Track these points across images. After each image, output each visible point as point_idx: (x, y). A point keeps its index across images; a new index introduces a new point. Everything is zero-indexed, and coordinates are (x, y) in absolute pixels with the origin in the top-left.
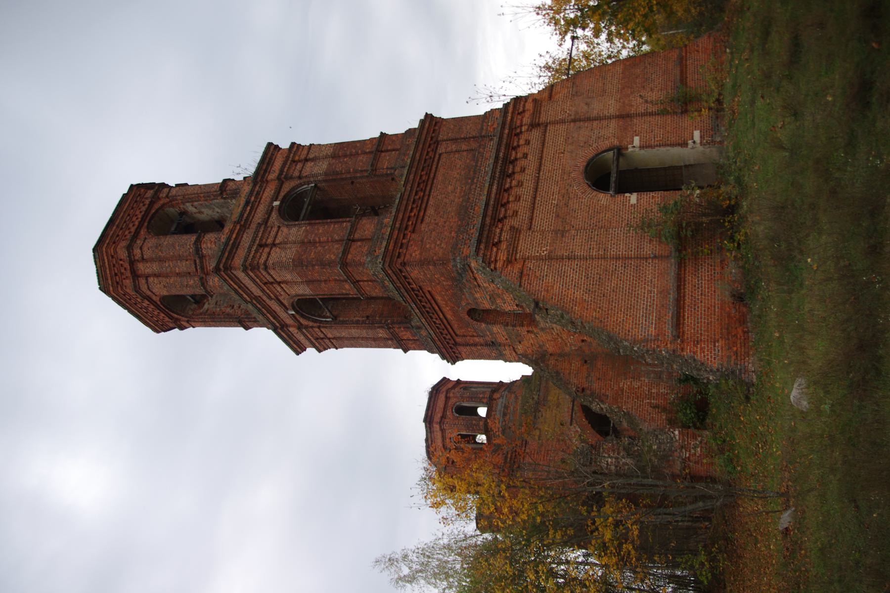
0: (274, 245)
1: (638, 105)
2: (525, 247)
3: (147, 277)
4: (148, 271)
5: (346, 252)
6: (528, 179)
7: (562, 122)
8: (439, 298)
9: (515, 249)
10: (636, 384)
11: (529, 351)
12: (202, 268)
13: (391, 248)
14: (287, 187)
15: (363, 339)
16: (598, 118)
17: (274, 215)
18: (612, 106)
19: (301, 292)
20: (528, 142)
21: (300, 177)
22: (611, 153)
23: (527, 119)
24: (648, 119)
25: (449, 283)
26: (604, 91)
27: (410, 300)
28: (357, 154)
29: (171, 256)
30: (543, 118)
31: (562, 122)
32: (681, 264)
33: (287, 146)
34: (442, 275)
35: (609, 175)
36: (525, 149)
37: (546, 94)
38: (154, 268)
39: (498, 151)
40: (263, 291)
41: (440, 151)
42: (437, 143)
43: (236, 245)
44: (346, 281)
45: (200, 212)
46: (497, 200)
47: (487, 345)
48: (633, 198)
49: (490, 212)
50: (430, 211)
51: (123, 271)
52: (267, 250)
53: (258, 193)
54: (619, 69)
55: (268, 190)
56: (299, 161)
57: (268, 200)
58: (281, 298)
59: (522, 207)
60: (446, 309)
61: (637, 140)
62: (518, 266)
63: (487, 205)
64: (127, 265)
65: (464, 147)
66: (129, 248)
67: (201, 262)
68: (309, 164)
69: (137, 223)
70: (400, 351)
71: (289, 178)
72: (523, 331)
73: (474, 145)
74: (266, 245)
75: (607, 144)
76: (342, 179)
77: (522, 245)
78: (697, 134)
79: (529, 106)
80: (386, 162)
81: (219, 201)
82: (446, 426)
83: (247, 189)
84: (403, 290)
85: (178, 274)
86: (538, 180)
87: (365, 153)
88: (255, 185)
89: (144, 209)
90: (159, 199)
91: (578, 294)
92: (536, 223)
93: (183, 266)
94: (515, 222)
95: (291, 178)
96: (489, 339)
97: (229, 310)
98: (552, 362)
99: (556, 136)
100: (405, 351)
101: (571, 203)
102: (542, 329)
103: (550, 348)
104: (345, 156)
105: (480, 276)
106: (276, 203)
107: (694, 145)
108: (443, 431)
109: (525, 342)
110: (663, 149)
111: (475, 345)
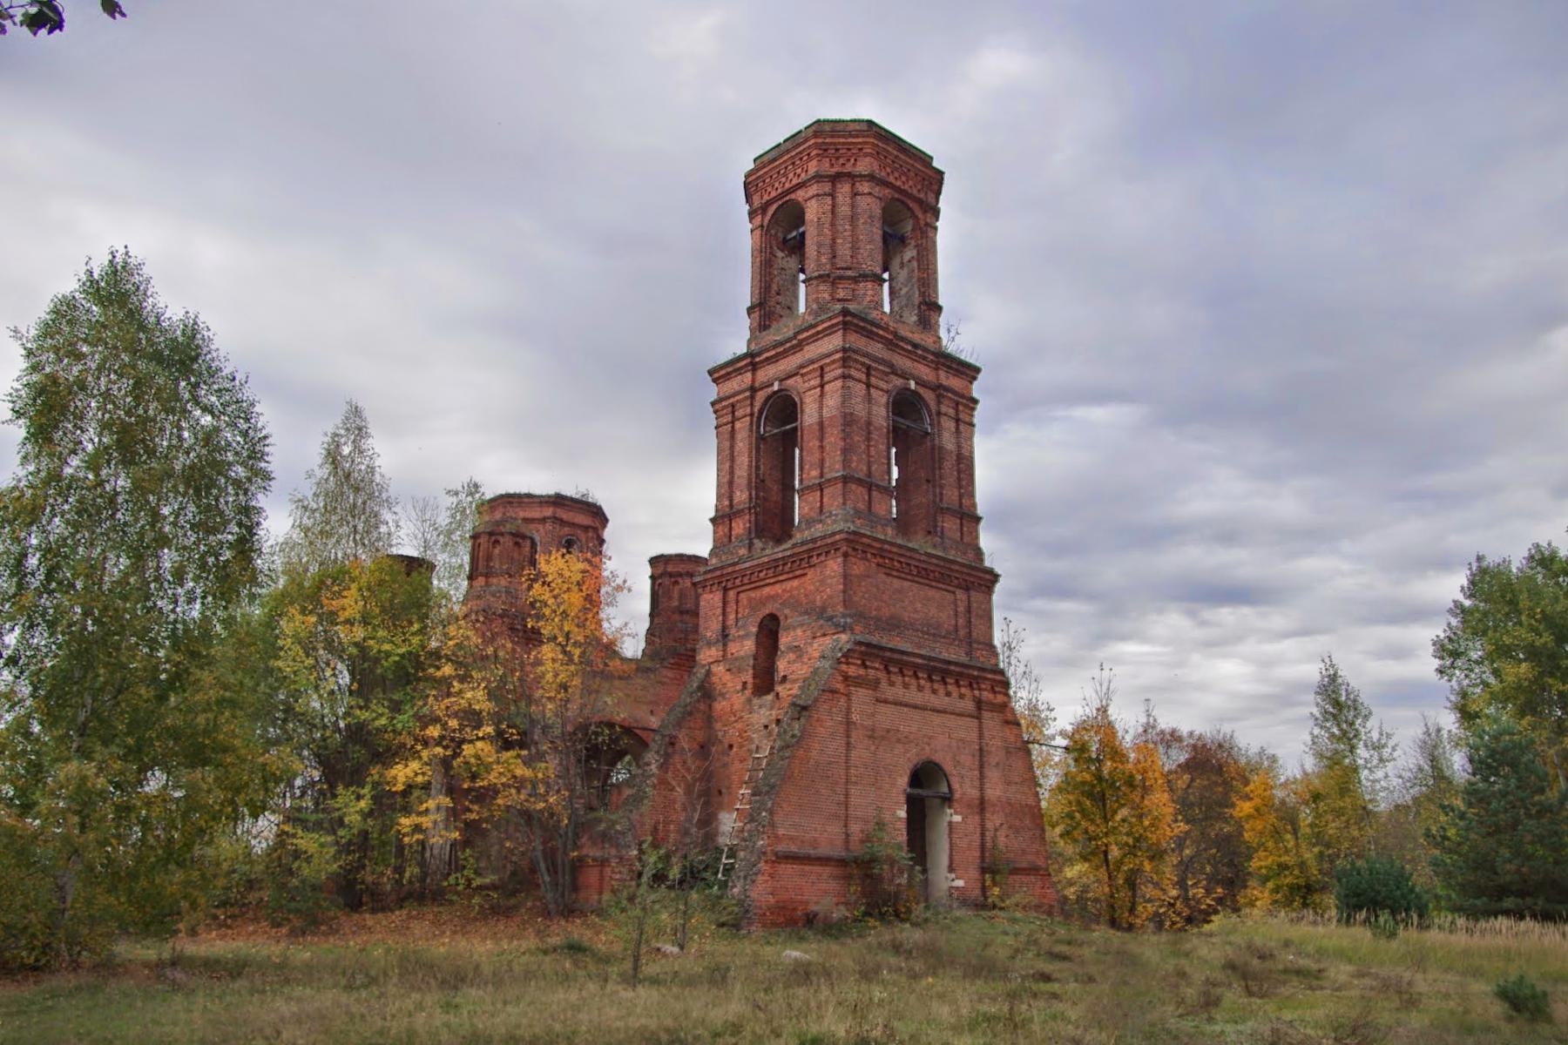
0: (868, 385)
1: (993, 821)
2: (861, 695)
3: (832, 195)
4: (840, 199)
5: (859, 482)
6: (925, 697)
7: (981, 736)
8: (796, 583)
9: (859, 685)
10: (678, 806)
11: (714, 679)
12: (841, 278)
13: (865, 540)
14: (929, 396)
15: (732, 472)
16: (982, 777)
17: (899, 382)
18: (994, 791)
19: (807, 410)
20: (962, 696)
21: (939, 413)
22: (946, 790)
23: (987, 695)
24: (978, 831)
25: (818, 604)
26: (1009, 783)
27: (796, 550)
28: (960, 487)
29: (844, 209)
30: (986, 715)
31: (981, 736)
32: (842, 862)
33: (975, 395)
34: (830, 597)
35: (926, 784)
36: (955, 694)
37: (1010, 717)
38: (844, 210)
39: (956, 664)
40: (812, 362)
41: (958, 591)
42: (967, 589)
43: (870, 335)
44: (822, 476)
45: (902, 265)
46: (907, 664)
47: (724, 628)
48: (903, 814)
49: (896, 656)
50: (897, 583)
51: (841, 161)
52: (864, 377)
53: (925, 358)
54: (1031, 801)
55: (927, 370)
56: (957, 411)
57: (916, 372)
58: (798, 378)
59: (897, 692)
60: (778, 588)
61: (957, 818)
62: (840, 687)
63: (903, 653)
64: (848, 168)
65: (961, 621)
66: (871, 177)
67: (849, 278)
68: (952, 425)
69: (898, 183)
70: (712, 514)
71: (939, 398)
72: (748, 676)
73: (962, 633)
74: (868, 375)
75: (956, 786)
76: (933, 469)
77: (862, 692)
78: (960, 883)
79: (1000, 699)
80: (950, 525)
81: (916, 299)
82: (549, 526)
83: (928, 341)
84: (811, 546)
85: (834, 240)
86: (924, 708)
87: (961, 496)
88: (933, 353)
89: (915, 192)
90: (925, 212)
91: (814, 753)
92: (882, 708)
93: (844, 251)
94: (884, 685)
95: (939, 403)
96: (733, 631)
97: (775, 287)
98: (702, 707)
99: (965, 729)
100: (713, 520)
101: (899, 746)
102: (749, 701)
103: (720, 706)
104: (959, 472)
105: (828, 640)
106: (912, 385)
107: (948, 878)
108: (543, 520)
109: (728, 677)
110: (946, 846)
111: (724, 614)
